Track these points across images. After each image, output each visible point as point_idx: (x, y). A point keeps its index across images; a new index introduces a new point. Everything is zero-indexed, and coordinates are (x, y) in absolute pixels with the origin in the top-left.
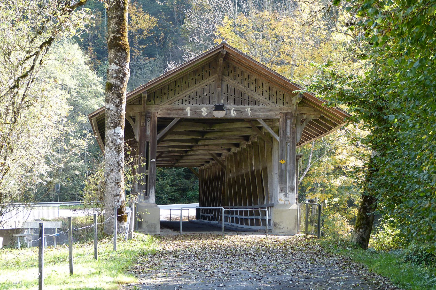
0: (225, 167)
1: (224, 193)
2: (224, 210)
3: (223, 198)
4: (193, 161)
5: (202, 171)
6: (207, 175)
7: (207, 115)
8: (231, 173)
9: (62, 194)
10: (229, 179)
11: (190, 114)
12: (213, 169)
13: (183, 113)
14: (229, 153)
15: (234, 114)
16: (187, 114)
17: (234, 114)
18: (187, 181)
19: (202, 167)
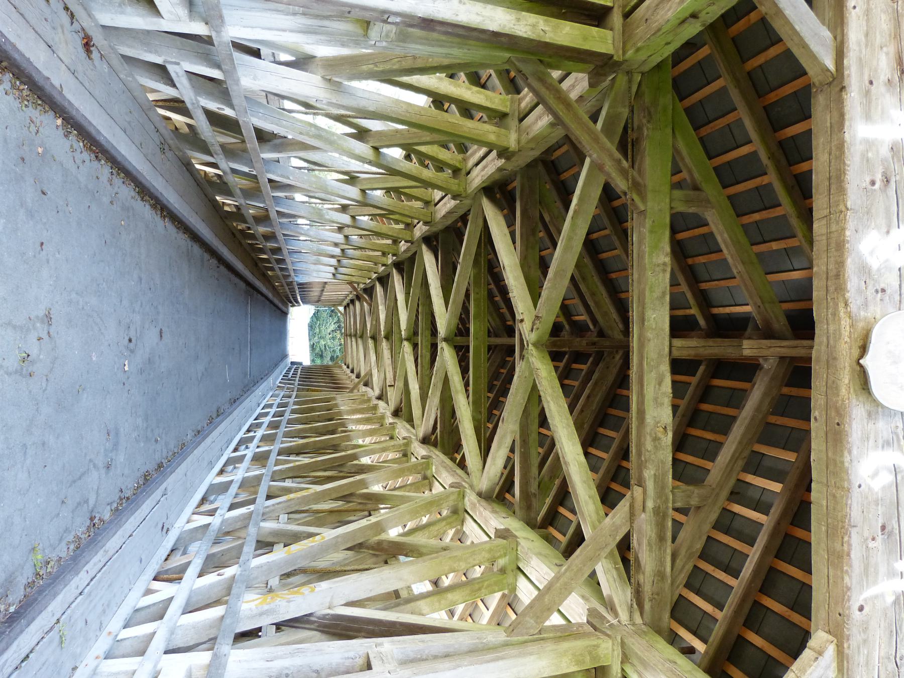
0: (352, 391)
1: (314, 391)
2: (719, 615)
3: (308, 390)
4: (355, 353)
5: (340, 367)
6: (336, 371)
7: (865, 270)
8: (343, 403)
9: (367, 24)
10: (334, 399)
11: (870, 144)
12: (344, 377)
13: (879, 88)
14: (374, 398)
15: (875, 474)
16: (868, 117)
17: (875, 474)
18: (329, 358)
19: (345, 367)
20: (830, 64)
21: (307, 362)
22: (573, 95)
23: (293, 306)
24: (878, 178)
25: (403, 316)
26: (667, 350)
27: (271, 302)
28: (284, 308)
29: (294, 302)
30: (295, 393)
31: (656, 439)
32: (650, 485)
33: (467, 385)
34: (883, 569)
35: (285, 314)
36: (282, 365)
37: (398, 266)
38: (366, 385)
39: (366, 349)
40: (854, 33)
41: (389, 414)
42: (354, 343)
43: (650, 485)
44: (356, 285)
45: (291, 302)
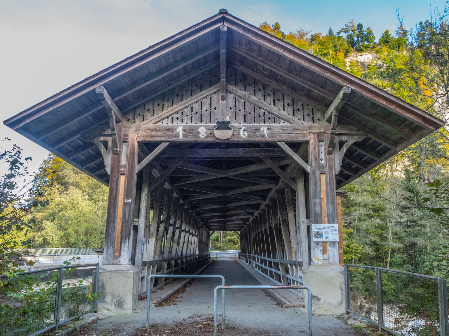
4: (234, 226)
11: (183, 136)
15: (245, 135)
20: (168, 143)
21: (239, 251)
22: (159, 175)
23: (209, 258)
24: (190, 134)
25: (213, 195)
26: (224, 150)
27: (208, 266)
28: (211, 262)
29: (208, 257)
30: (252, 255)
31: (247, 152)
32: (259, 154)
33: (239, 188)
34: (262, 133)
35: (214, 261)
36: (239, 262)
37: (185, 198)
38: (248, 221)
39: (231, 221)
40: (163, 139)
41: (258, 212)
42: (229, 226)
43: (259, 154)
44: (200, 225)
45: (207, 259)
